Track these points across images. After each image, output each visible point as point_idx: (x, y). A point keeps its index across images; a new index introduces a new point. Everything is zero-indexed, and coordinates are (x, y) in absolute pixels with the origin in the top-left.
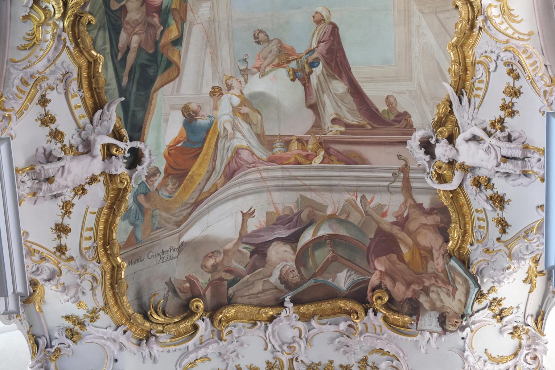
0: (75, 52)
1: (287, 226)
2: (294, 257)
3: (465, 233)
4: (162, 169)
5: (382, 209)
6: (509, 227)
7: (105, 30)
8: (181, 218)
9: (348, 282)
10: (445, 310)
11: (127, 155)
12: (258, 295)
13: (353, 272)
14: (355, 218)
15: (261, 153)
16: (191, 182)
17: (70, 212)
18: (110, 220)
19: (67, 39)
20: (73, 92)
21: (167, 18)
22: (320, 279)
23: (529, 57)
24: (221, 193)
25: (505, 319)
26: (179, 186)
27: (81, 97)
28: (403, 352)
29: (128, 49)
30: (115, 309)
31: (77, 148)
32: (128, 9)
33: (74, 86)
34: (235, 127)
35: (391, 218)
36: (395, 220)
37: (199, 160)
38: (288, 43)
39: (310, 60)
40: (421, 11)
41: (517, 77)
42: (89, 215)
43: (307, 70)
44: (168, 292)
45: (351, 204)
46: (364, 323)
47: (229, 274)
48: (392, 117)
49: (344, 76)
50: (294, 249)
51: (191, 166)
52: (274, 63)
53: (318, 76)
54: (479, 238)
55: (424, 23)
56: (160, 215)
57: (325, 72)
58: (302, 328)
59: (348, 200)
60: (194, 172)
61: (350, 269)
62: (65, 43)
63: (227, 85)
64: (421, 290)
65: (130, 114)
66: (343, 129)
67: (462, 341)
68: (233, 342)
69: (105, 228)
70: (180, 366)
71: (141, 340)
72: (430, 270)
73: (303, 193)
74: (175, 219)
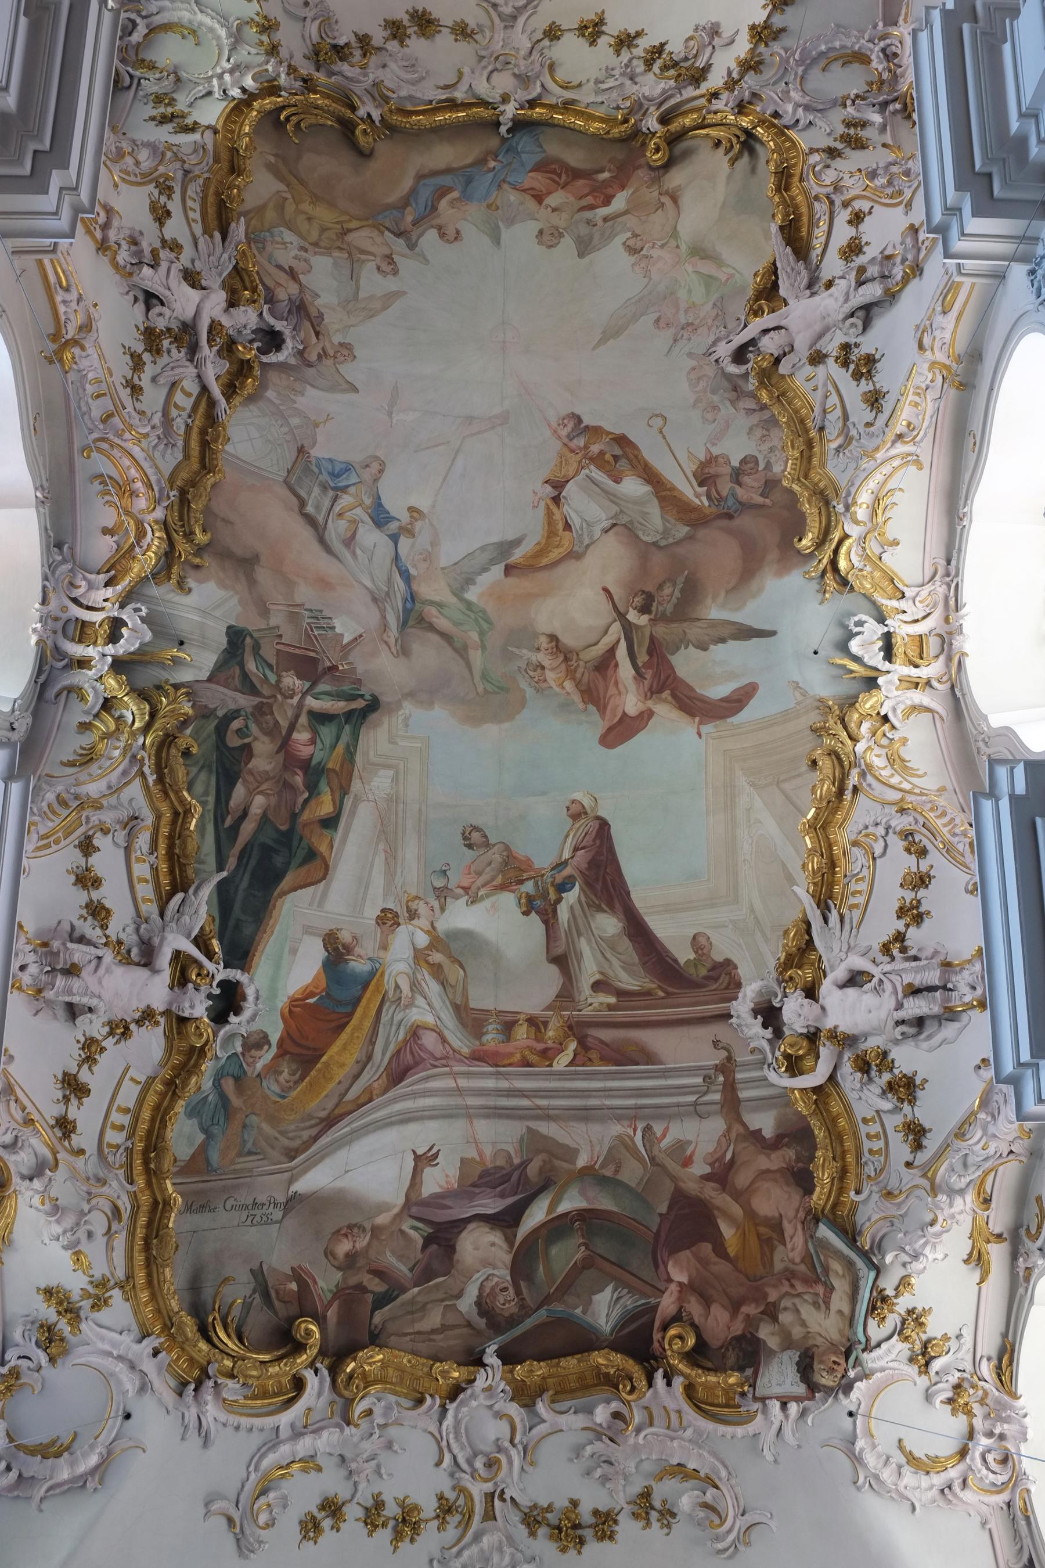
0: (155, 790)
1: (499, 1189)
2: (508, 1258)
3: (844, 1172)
4: (275, 1037)
5: (684, 1150)
6: (928, 1135)
7: (210, 772)
8: (296, 1143)
9: (614, 1314)
10: (811, 1342)
11: (217, 991)
12: (432, 1337)
13: (626, 1291)
14: (632, 1174)
15: (459, 1041)
16: (324, 1076)
17: (95, 1061)
18: (166, 1103)
19: (146, 761)
20: (139, 853)
21: (318, 782)
22: (558, 1307)
23: (944, 814)
24: (378, 1108)
25: (936, 1365)
26: (302, 1078)
27: (151, 866)
28: (726, 1467)
29: (245, 814)
30: (144, 1296)
31: (129, 952)
32: (255, 752)
33: (143, 840)
34: (415, 986)
35: (700, 1168)
36: (708, 1170)
37: (344, 1036)
38: (521, 850)
39: (559, 879)
40: (753, 785)
41: (923, 853)
42: (127, 1082)
43: (552, 896)
44: (254, 1291)
45: (624, 1143)
46: (646, 1408)
47: (377, 1280)
48: (703, 972)
49: (617, 905)
50: (510, 1241)
51: (328, 1045)
52: (495, 883)
53: (572, 907)
54: (873, 1174)
55: (758, 803)
56: (260, 1129)
57: (583, 899)
58: (517, 1420)
59: (619, 1138)
60: (331, 1057)
61: (620, 1283)
62: (142, 765)
63: (409, 910)
64: (762, 1313)
65: (232, 923)
66: (612, 1000)
67: (850, 1420)
68: (371, 1435)
69: (153, 1120)
70: (256, 1469)
71: (184, 1384)
72: (778, 1266)
73: (533, 1125)
74: (286, 1142)
